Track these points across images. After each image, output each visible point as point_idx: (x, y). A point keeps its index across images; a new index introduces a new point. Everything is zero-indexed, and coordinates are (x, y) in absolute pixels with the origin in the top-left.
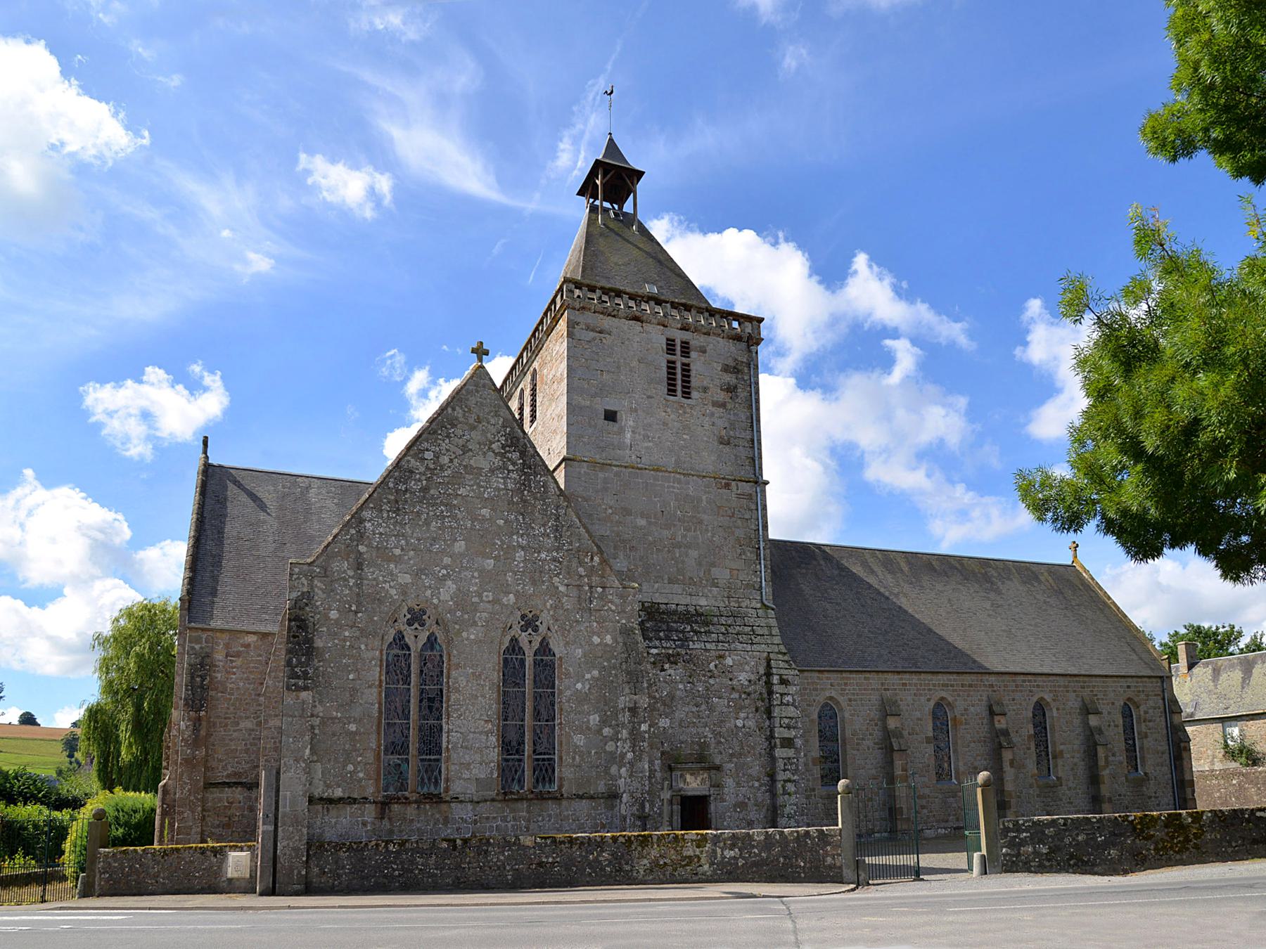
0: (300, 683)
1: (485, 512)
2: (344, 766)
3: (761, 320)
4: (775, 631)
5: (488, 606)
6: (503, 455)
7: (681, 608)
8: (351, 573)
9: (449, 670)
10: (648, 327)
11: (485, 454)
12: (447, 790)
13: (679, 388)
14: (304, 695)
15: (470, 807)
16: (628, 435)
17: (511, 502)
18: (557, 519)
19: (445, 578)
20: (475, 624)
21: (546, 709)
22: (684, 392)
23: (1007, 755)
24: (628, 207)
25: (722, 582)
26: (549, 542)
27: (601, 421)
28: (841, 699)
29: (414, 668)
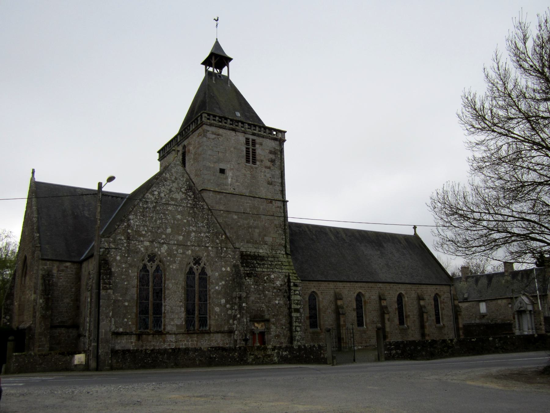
0: (108, 286)
1: (179, 217)
2: (123, 319)
3: (285, 132)
4: (292, 264)
5: (180, 255)
6: (186, 194)
7: (252, 254)
8: (125, 241)
9: (165, 281)
10: (238, 133)
11: (178, 193)
12: (164, 329)
13: (251, 160)
14: (109, 291)
15: (174, 336)
16: (230, 180)
17: (189, 213)
18: (208, 220)
19: (163, 243)
20: (175, 262)
21: (204, 296)
22: (253, 162)
23: (387, 316)
24: (224, 72)
25: (269, 243)
26: (205, 229)
27: (218, 174)
28: (318, 292)
29: (151, 280)
